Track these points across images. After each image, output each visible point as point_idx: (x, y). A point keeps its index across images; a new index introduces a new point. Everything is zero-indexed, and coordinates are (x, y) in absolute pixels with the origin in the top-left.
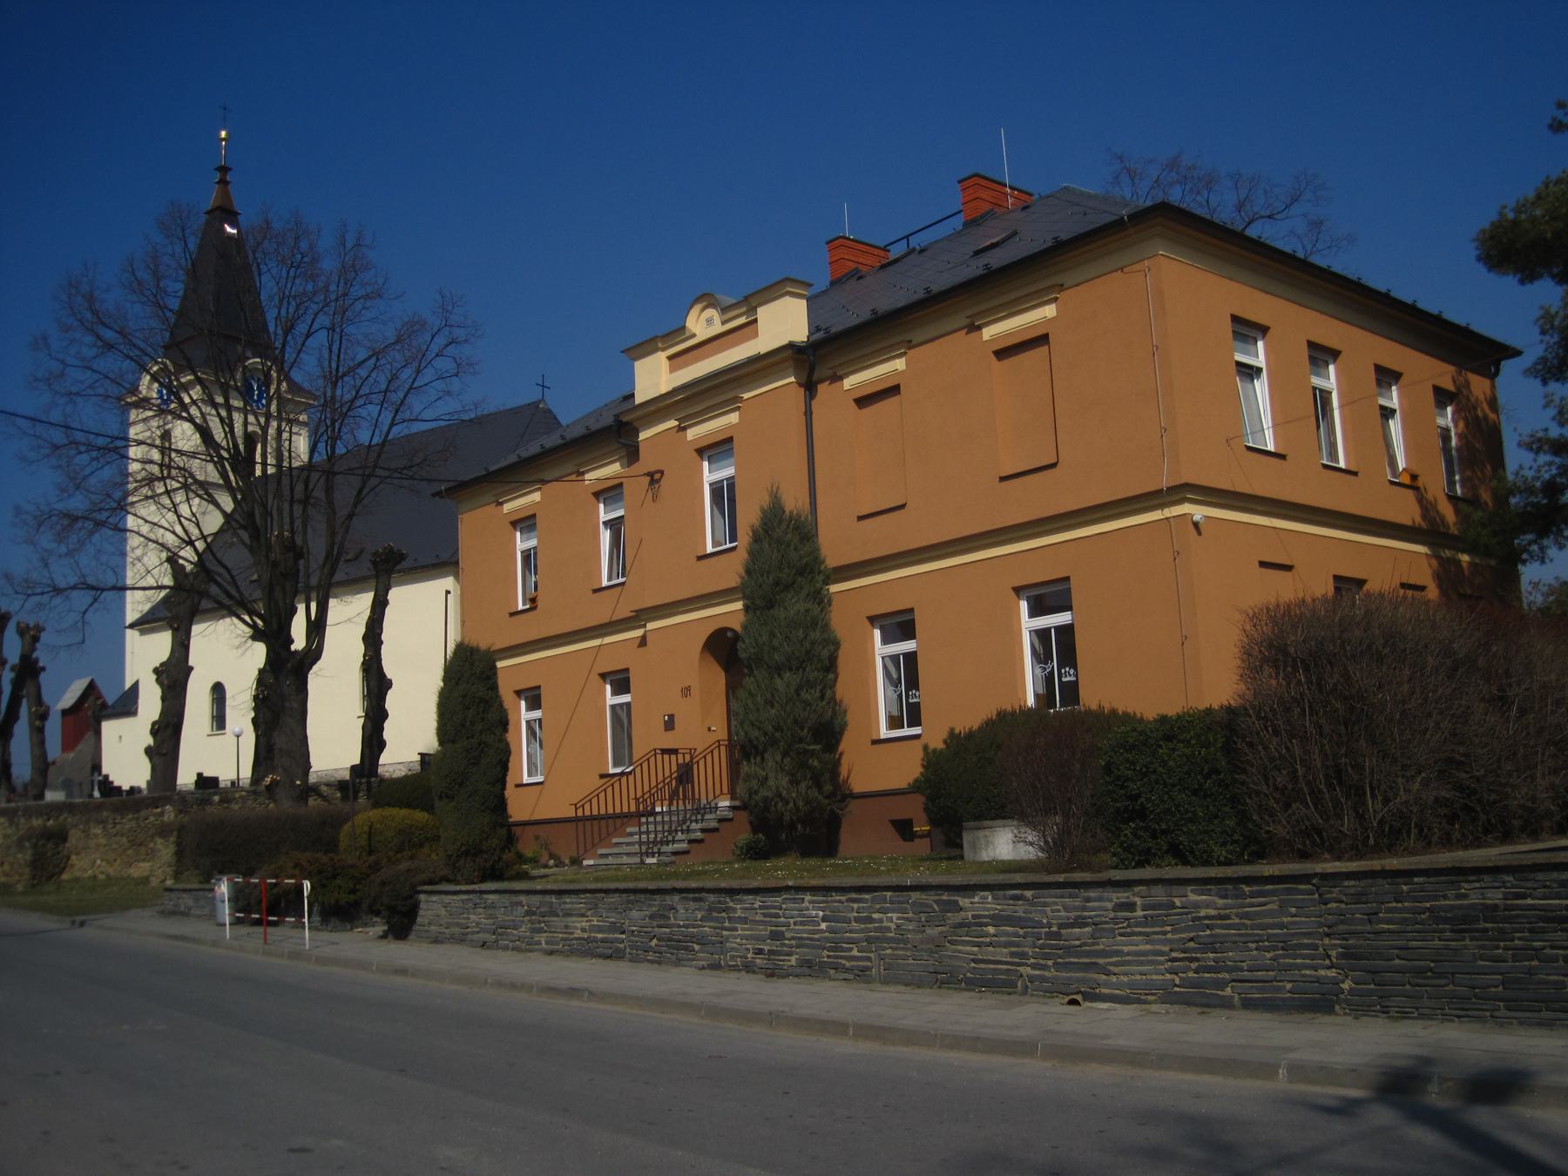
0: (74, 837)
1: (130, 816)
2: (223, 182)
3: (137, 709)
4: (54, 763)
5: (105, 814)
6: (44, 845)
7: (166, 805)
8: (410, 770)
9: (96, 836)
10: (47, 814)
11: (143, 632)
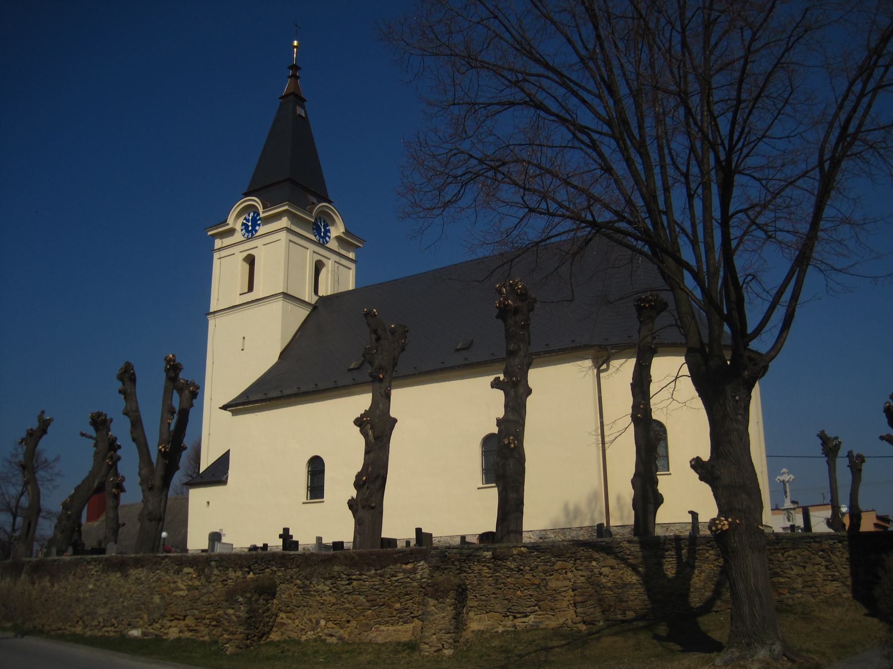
0: (286, 592)
1: (373, 572)
2: (295, 77)
3: (227, 478)
4: (124, 525)
5: (336, 568)
6: (257, 600)
7: (419, 561)
8: (541, 538)
9: (320, 593)
10: (249, 567)
11: (235, 413)
